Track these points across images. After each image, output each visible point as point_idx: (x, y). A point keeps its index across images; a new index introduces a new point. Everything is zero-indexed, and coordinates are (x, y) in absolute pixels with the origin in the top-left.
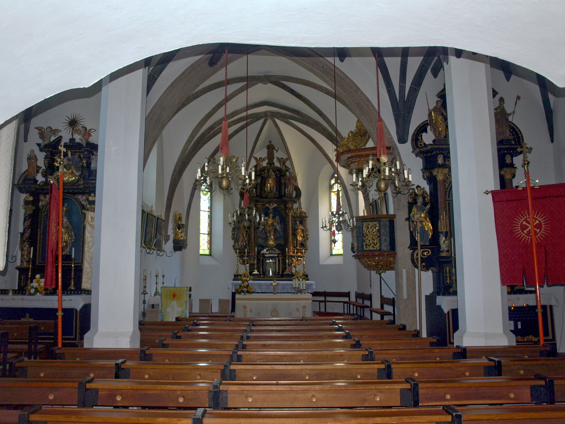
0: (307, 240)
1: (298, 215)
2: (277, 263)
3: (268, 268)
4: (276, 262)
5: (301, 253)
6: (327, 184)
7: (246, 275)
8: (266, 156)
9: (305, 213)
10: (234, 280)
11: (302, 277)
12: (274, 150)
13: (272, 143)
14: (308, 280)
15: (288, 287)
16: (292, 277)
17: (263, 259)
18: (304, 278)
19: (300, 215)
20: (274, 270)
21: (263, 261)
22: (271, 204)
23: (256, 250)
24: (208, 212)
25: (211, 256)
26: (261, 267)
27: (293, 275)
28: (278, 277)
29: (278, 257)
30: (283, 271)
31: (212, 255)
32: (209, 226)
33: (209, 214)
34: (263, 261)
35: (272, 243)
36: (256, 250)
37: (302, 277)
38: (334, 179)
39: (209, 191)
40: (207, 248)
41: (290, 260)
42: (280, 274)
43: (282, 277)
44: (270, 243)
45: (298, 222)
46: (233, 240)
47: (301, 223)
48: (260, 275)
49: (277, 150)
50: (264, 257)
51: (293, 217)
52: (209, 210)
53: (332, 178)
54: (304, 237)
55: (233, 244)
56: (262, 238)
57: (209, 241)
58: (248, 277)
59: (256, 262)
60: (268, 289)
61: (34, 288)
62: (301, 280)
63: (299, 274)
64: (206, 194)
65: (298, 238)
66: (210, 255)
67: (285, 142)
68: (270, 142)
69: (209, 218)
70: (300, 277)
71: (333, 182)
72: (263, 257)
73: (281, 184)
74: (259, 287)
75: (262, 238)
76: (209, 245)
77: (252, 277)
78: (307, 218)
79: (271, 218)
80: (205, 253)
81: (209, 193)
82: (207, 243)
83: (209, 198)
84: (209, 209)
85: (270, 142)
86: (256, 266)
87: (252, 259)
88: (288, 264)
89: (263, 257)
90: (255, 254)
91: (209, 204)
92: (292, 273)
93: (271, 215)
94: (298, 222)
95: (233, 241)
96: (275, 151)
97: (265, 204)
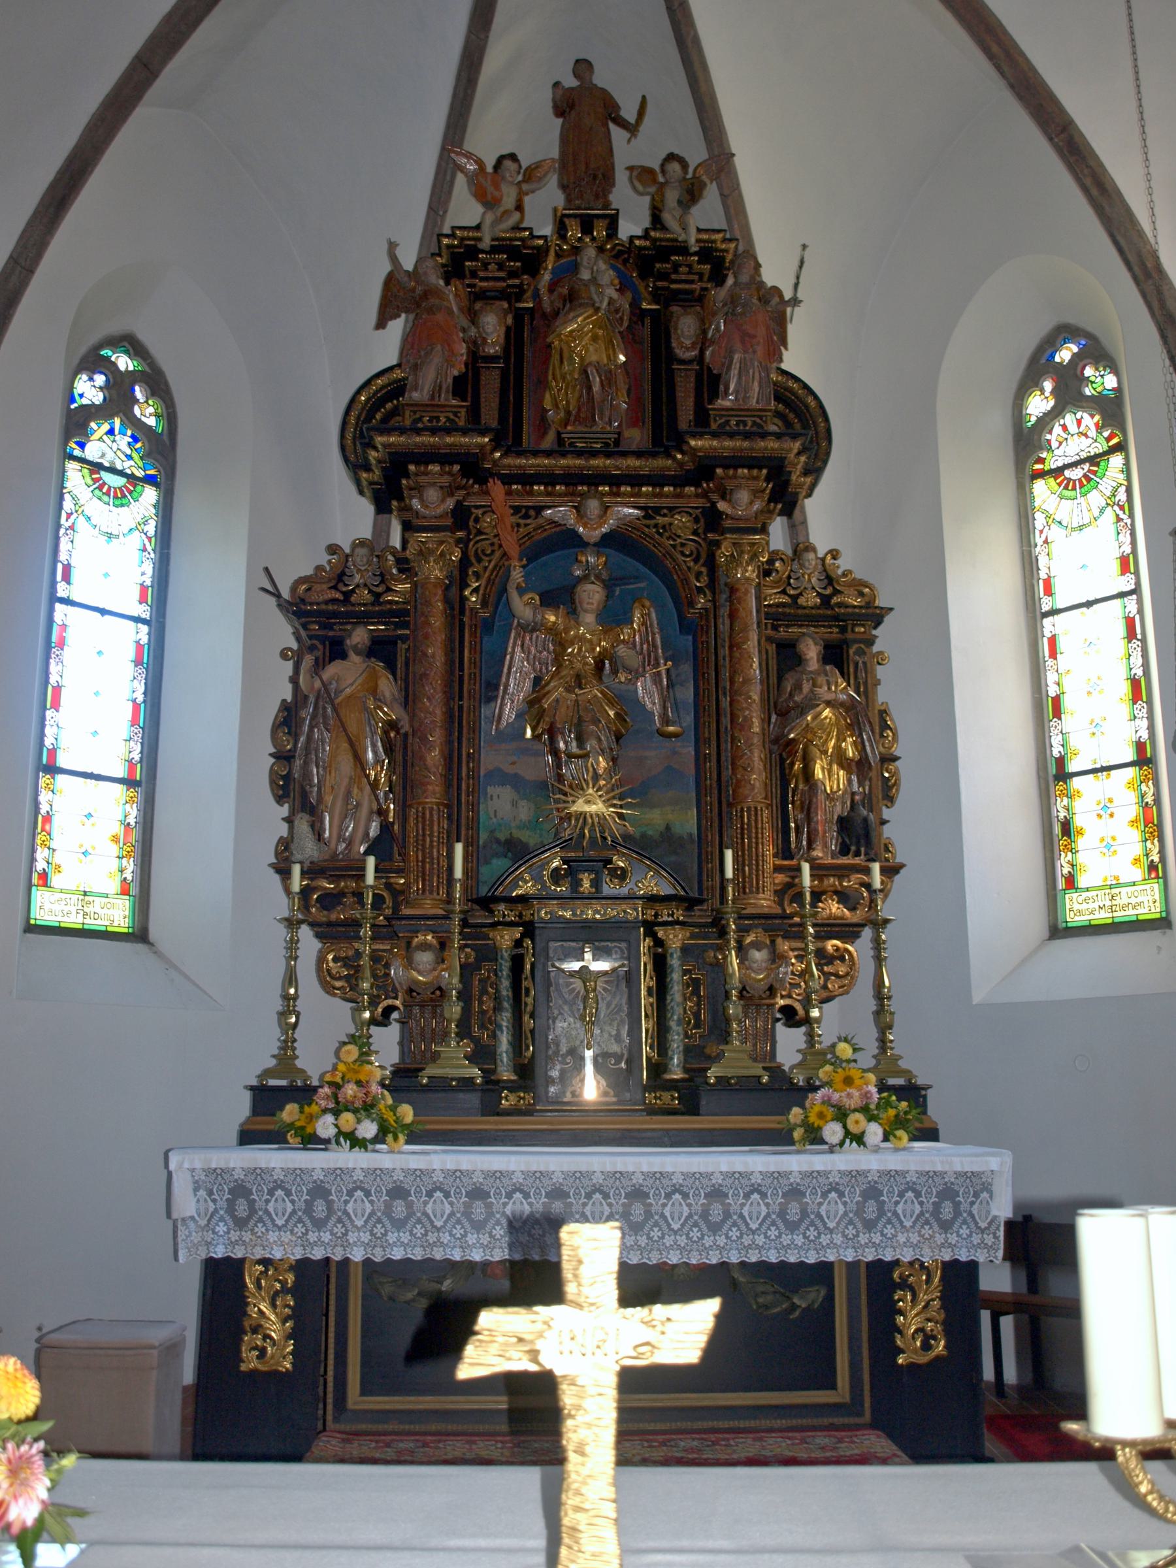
0: (890, 799)
1: (811, 599)
2: (645, 983)
3: (560, 1025)
4: (630, 979)
5: (843, 897)
6: (998, 424)
7: (350, 1090)
8: (555, 153)
9: (859, 586)
10: (247, 1137)
11: (884, 1105)
12: (612, 126)
13: (600, 79)
14: (930, 1134)
15: (755, 1209)
16: (785, 1111)
17: (518, 943)
18: (899, 1122)
19: (826, 600)
20: (615, 1048)
21: (517, 962)
22: (593, 506)
23: (458, 873)
24: (137, 620)
25: (140, 947)
26: (505, 1019)
27: (799, 1093)
28: (652, 1111)
29: (650, 932)
30: (697, 1057)
31: (153, 934)
32: (134, 721)
33: (144, 639)
34: (517, 962)
35: (597, 807)
36: (458, 873)
37: (884, 1105)
38: (1048, 385)
39: (150, 480)
40: (115, 886)
41: (759, 956)
42: (673, 1085)
43: (691, 1107)
44: (580, 806)
45: (812, 652)
46: (280, 800)
47: (835, 655)
48: (492, 1085)
49: (632, 120)
50: (529, 929)
51: (774, 617)
52: (143, 611)
53: (1029, 383)
54: (859, 767)
55: (283, 830)
56: (515, 781)
57: (134, 837)
58: (367, 1108)
59: (452, 979)
60: (478, 1226)
61: (865, 1201)
62: (874, 1132)
63: (848, 1081)
64: (120, 497)
65: (819, 773)
66: (140, 935)
67: (697, 41)
68: (583, 67)
69: (138, 662)
70: (865, 1109)
71: (1038, 405)
72: (517, 933)
73: (672, 358)
74: (231, 1208)
75: (515, 781)
76: (130, 866)
77: (407, 1112)
78: (878, 622)
79: (590, 618)
80: (99, 924)
81: (150, 495)
82: (114, 850)
83: (151, 528)
84: (143, 600)
85: (583, 67)
86: (454, 1010)
87: (425, 947)
88: (743, 991)
89: (517, 933)
90: (449, 900)
91: (149, 568)
92: (776, 1071)
93: (592, 595)
94: (812, 652)
95: (285, 810)
96: (617, 134)
97: (539, 510)
